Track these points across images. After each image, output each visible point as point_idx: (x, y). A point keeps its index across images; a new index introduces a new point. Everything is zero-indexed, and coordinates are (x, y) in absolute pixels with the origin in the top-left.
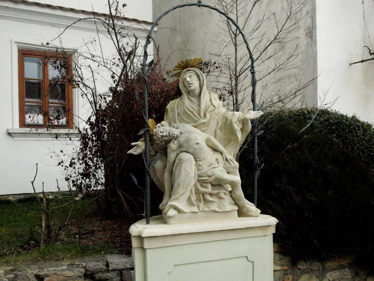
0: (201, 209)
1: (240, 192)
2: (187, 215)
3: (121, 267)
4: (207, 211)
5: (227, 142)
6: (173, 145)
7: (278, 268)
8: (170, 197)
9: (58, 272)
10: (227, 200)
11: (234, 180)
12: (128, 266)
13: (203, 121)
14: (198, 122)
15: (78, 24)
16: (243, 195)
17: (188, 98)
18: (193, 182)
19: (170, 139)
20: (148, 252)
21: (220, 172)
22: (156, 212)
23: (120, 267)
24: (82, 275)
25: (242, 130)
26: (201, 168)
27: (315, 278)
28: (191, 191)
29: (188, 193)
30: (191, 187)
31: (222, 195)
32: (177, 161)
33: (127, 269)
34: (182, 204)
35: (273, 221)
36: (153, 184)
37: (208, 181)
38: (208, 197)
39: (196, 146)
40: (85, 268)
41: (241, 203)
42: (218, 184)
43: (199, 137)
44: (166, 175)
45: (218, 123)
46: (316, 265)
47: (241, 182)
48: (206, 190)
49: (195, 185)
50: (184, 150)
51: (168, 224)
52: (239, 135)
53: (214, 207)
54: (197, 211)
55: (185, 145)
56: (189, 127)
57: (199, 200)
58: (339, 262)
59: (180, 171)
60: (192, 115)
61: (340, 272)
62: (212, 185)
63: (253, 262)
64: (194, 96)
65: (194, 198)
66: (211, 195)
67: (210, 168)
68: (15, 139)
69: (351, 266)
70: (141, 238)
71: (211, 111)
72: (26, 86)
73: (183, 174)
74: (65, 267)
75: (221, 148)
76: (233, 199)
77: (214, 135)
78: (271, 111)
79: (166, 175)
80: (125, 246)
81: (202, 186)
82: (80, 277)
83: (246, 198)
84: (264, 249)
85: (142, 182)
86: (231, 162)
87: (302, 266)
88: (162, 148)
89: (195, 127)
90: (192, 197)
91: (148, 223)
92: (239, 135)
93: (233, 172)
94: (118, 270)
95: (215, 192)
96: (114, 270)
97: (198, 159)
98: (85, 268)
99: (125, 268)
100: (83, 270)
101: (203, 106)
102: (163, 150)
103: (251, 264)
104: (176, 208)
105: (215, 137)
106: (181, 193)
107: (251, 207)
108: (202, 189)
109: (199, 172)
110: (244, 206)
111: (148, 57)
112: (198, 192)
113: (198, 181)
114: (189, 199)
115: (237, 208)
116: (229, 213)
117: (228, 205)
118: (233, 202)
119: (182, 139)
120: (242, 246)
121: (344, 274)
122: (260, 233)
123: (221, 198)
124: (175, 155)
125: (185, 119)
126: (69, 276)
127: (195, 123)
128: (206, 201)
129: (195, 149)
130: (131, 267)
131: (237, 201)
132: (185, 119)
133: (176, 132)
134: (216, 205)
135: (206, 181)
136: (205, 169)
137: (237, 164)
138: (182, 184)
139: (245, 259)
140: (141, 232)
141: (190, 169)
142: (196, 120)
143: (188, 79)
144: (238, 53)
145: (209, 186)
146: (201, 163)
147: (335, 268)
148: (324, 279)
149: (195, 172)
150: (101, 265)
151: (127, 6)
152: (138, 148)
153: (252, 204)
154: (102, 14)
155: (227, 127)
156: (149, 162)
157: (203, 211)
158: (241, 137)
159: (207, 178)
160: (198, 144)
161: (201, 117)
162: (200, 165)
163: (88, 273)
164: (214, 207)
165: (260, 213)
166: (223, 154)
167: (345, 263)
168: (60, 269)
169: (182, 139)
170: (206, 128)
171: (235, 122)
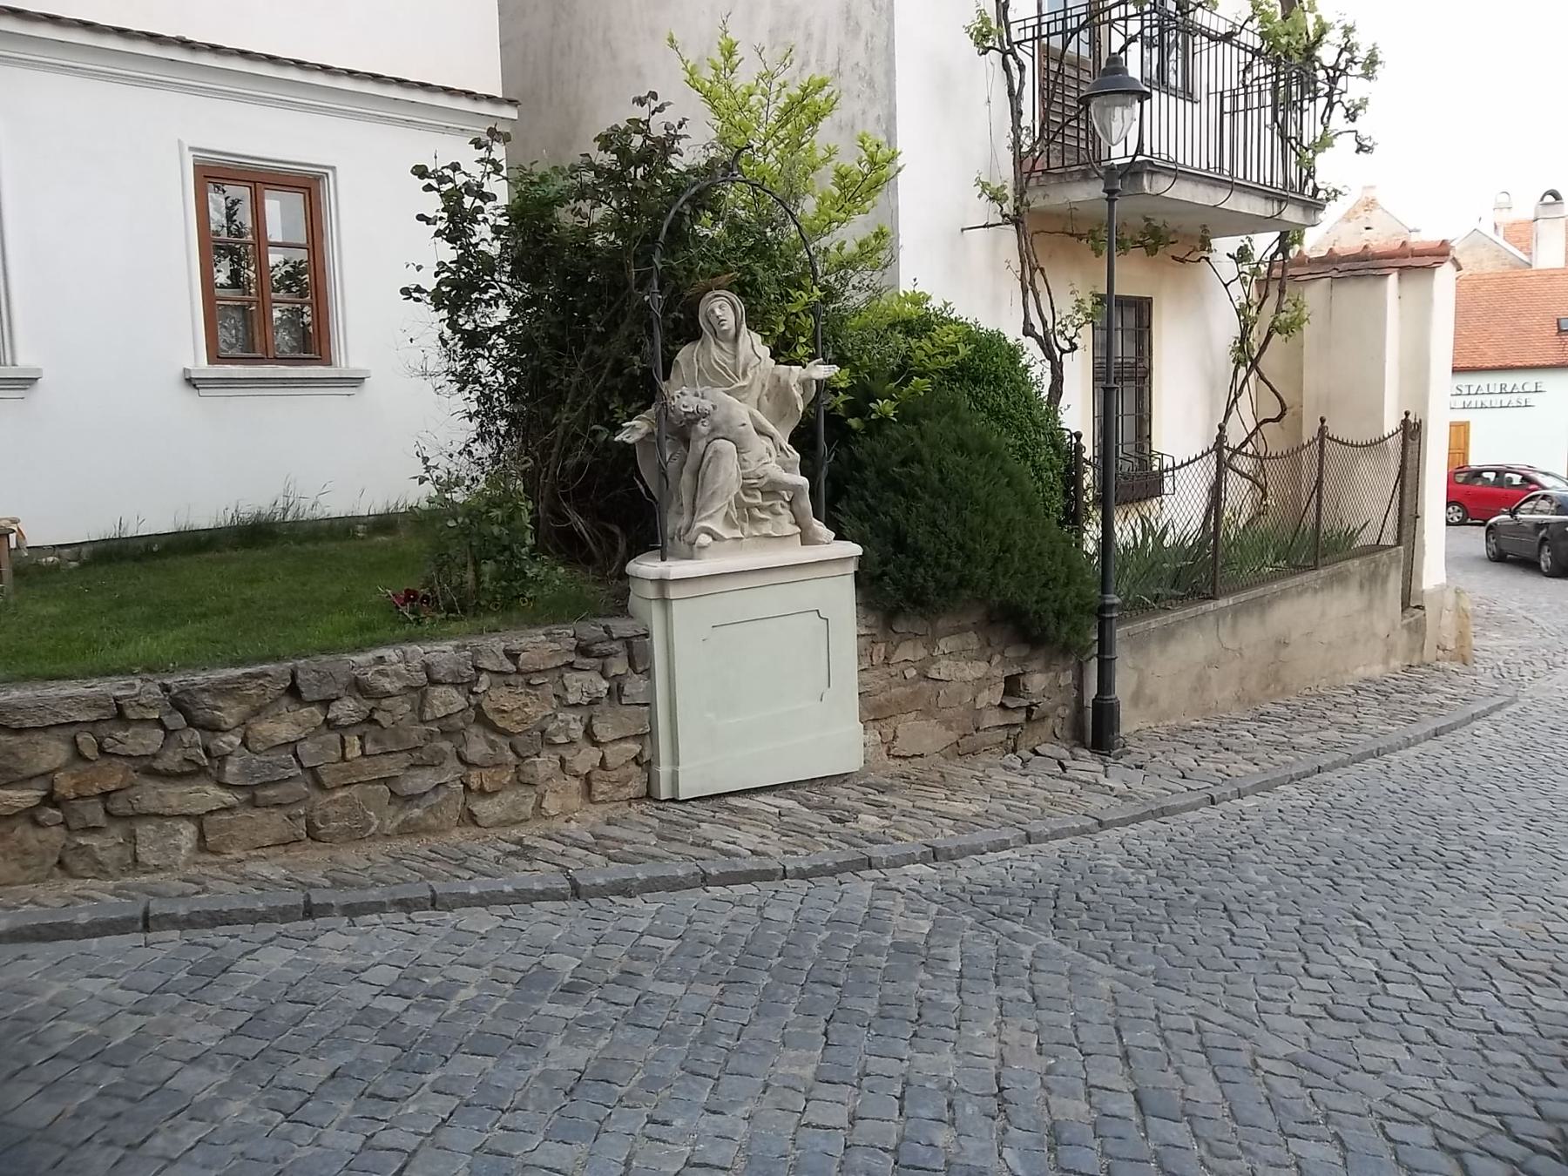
1: (807, 503)
5: (778, 419)
6: (703, 428)
7: (863, 632)
10: (786, 515)
13: (745, 383)
18: (736, 489)
19: (699, 415)
20: (676, 607)
21: (775, 471)
32: (709, 454)
34: (717, 526)
35: (855, 549)
38: (756, 512)
42: (772, 490)
43: (742, 412)
44: (686, 478)
46: (920, 626)
53: (767, 529)
55: (724, 427)
56: (720, 393)
59: (717, 471)
64: (726, 340)
65: (734, 514)
66: (760, 508)
68: (202, 392)
69: (977, 628)
73: (721, 478)
75: (772, 428)
79: (686, 478)
84: (841, 594)
87: (901, 626)
88: (682, 430)
89: (728, 393)
96: (620, 638)
101: (741, 359)
104: (709, 532)
107: (819, 527)
108: (746, 499)
110: (810, 526)
112: (739, 504)
119: (717, 417)
120: (812, 592)
122: (837, 570)
128: (754, 520)
129: (740, 433)
133: (707, 405)
134: (769, 525)
136: (753, 466)
143: (718, 312)
144: (1127, 1164)
146: (745, 456)
152: (634, 431)
155: (780, 392)
164: (767, 529)
167: (967, 622)
169: (717, 417)
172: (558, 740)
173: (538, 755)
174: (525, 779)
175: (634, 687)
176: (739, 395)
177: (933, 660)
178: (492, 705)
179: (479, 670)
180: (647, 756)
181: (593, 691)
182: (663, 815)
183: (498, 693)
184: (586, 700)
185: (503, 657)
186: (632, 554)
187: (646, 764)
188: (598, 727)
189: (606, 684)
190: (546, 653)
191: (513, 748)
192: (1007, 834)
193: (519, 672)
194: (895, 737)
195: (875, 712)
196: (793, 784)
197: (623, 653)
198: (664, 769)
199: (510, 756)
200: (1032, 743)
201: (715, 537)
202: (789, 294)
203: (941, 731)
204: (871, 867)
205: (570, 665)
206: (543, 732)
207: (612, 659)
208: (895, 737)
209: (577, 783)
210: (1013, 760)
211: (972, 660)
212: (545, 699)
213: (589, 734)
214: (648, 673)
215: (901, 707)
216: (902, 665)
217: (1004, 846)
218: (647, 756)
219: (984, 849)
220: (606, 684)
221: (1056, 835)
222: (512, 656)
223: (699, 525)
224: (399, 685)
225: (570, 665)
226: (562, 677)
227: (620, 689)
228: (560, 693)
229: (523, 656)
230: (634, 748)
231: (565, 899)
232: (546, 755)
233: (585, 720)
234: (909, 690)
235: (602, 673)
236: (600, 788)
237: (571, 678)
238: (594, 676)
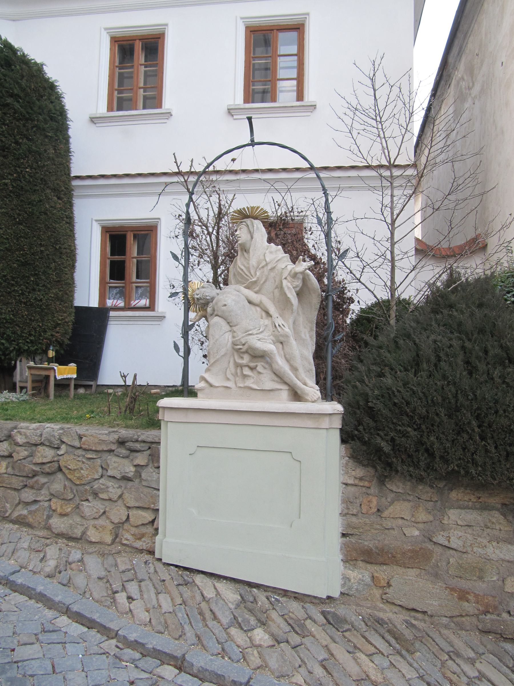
11: (265, 349)
15: (168, 189)
24: (115, 441)
39: (224, 307)
53: (249, 383)
57: (235, 375)
58: (479, 498)
61: (481, 515)
67: (244, 335)
71: (263, 267)
72: (314, 274)
78: (486, 272)
116: (272, 393)
121: (490, 521)
122: (310, 423)
125: (240, 279)
129: (223, 311)
132: (240, 279)
134: (252, 380)
146: (235, 328)
147: (470, 506)
151: (236, 161)
154: (112, 175)
159: (241, 347)
160: (225, 305)
164: (249, 383)
171: (286, 278)
184: (119, 476)
205: (111, 451)
224: (25, 441)
225: (111, 451)
237: (112, 460)
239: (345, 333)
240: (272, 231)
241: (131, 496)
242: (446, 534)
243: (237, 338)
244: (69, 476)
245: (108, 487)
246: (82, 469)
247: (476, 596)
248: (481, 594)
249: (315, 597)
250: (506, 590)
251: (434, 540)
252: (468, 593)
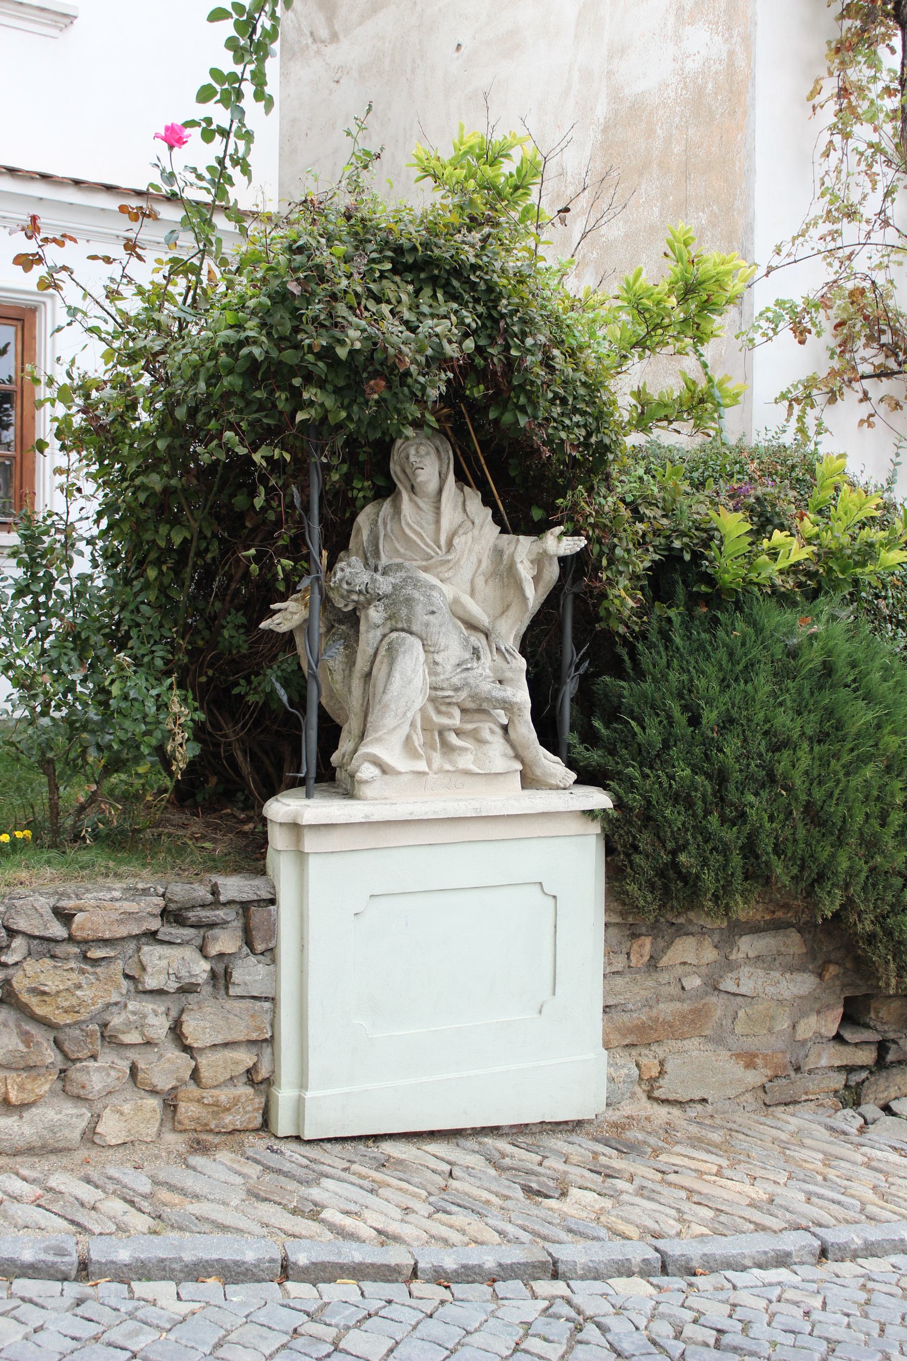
0: (435, 766)
1: (526, 731)
2: (402, 777)
3: (245, 897)
4: (448, 771)
6: (375, 614)
8: (362, 736)
9: (105, 903)
10: (497, 744)
12: (266, 895)
14: (432, 557)
16: (534, 735)
17: (411, 500)
18: (420, 700)
20: (313, 863)
22: (329, 778)
23: (245, 895)
24: (158, 911)
25: (536, 579)
26: (439, 669)
27: (711, 948)
28: (413, 724)
29: (405, 729)
30: (414, 712)
31: (486, 735)
33: (259, 901)
36: (323, 715)
37: (454, 700)
38: (453, 738)
40: (163, 895)
41: (528, 755)
42: (478, 708)
44: (357, 684)
45: (480, 561)
47: (530, 705)
48: (445, 721)
49: (422, 710)
50: (400, 626)
51: (359, 799)
52: (530, 591)
54: (426, 769)
60: (419, 542)
62: (464, 711)
63: (555, 897)
65: (418, 739)
70: (295, 828)
74: (117, 894)
76: (513, 747)
77: (469, 589)
79: (357, 684)
80: (253, 853)
81: (439, 712)
82: (154, 915)
83: (543, 743)
84: (579, 864)
85: (300, 702)
86: (507, 655)
90: (415, 737)
91: (308, 796)
92: (530, 591)
93: (512, 680)
94: (242, 903)
95: (470, 726)
97: (432, 649)
98: (163, 895)
99: (255, 898)
100: (161, 902)
102: (350, 621)
103: (551, 900)
104: (377, 763)
105: (472, 594)
106: (392, 726)
107: (553, 766)
109: (433, 678)
111: (59, 1283)
113: (432, 700)
114: (408, 738)
115: (520, 767)
116: (501, 778)
117: (497, 755)
118: (511, 752)
123: (481, 741)
124: (379, 637)
125: (402, 550)
126: (130, 913)
127: (427, 560)
128: (447, 748)
130: (270, 896)
131: (519, 749)
135: (448, 700)
137: (522, 663)
138: (393, 706)
139: (538, 887)
140: (298, 814)
141: (414, 671)
142: (428, 554)
145: (457, 712)
148: (734, 952)
149: (424, 679)
150: (202, 892)
153: (557, 759)
156: (319, 650)
157: (441, 771)
158: (534, 597)
161: (439, 547)
162: (436, 663)
163: (172, 906)
164: (466, 762)
165: (576, 782)
166: (491, 639)
168: (109, 896)
170: (450, 574)
172: (127, 1039)
173: (94, 1057)
174: (73, 1089)
175: (249, 974)
176: (452, 579)
177: (729, 966)
178: (26, 982)
179: (12, 933)
180: (263, 1073)
181: (183, 973)
182: (273, 1160)
183: (38, 967)
184: (172, 986)
185: (50, 916)
186: (271, 790)
187: (261, 1083)
188: (190, 1027)
189: (206, 966)
190: (115, 916)
191: (57, 1043)
192: (792, 1242)
193: (71, 939)
194: (661, 1073)
195: (629, 1033)
196: (494, 1131)
197: (238, 924)
198: (285, 1094)
199: (50, 1055)
200: (883, 1097)
201: (384, 769)
202: (521, 444)
203: (737, 1070)
204: (555, 1276)
205: (152, 936)
206: (105, 1025)
207: (216, 931)
208: (661, 1073)
209: (153, 1103)
210: (849, 1120)
211: (791, 969)
212: (110, 978)
213: (176, 1031)
214: (271, 954)
215: (675, 1030)
216: (680, 970)
217: (782, 1260)
218: (263, 1073)
219: (748, 1262)
220: (206, 966)
221: (871, 1250)
222: (64, 917)
223: (363, 750)
225: (152, 936)
226: (139, 950)
227: (227, 974)
228: (134, 973)
229: (79, 918)
230: (245, 1058)
231: (65, 1279)
232: (107, 1057)
233: (174, 1013)
234: (686, 1007)
235: (202, 949)
236: (188, 1110)
237: (152, 954)
238: (189, 953)
239: (242, 451)
240: (796, 736)
241: (202, 1023)
242: (734, 975)
243: (442, 677)
244: (40, 1011)
245: (145, 1017)
246: (79, 987)
247: (765, 1057)
248: (770, 1052)
249: (566, 1122)
250: (798, 1038)
251: (721, 987)
252: (756, 1056)
